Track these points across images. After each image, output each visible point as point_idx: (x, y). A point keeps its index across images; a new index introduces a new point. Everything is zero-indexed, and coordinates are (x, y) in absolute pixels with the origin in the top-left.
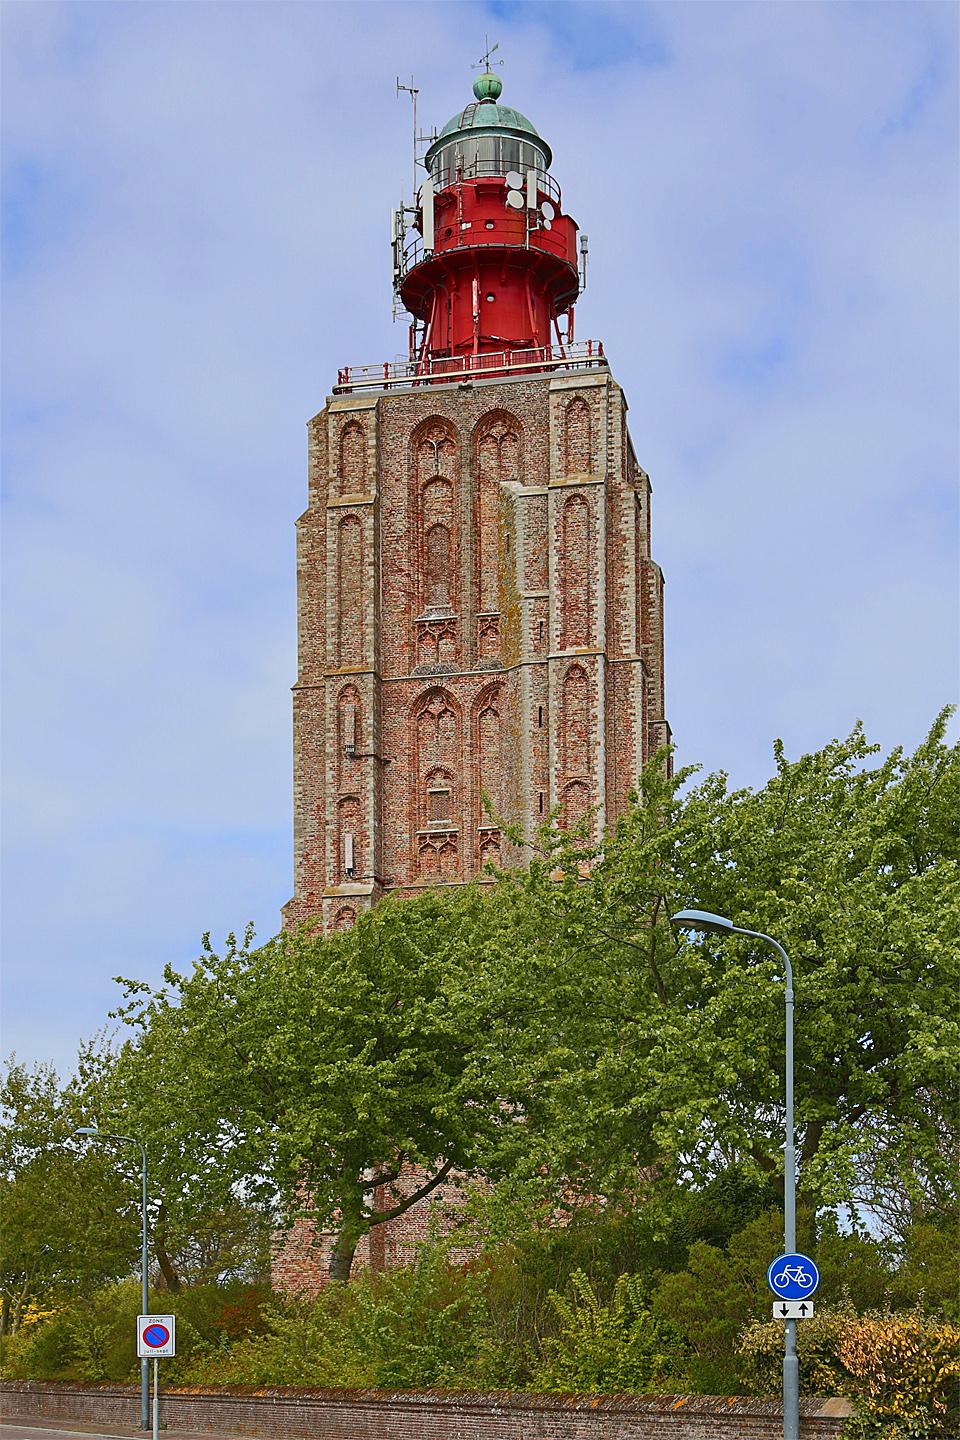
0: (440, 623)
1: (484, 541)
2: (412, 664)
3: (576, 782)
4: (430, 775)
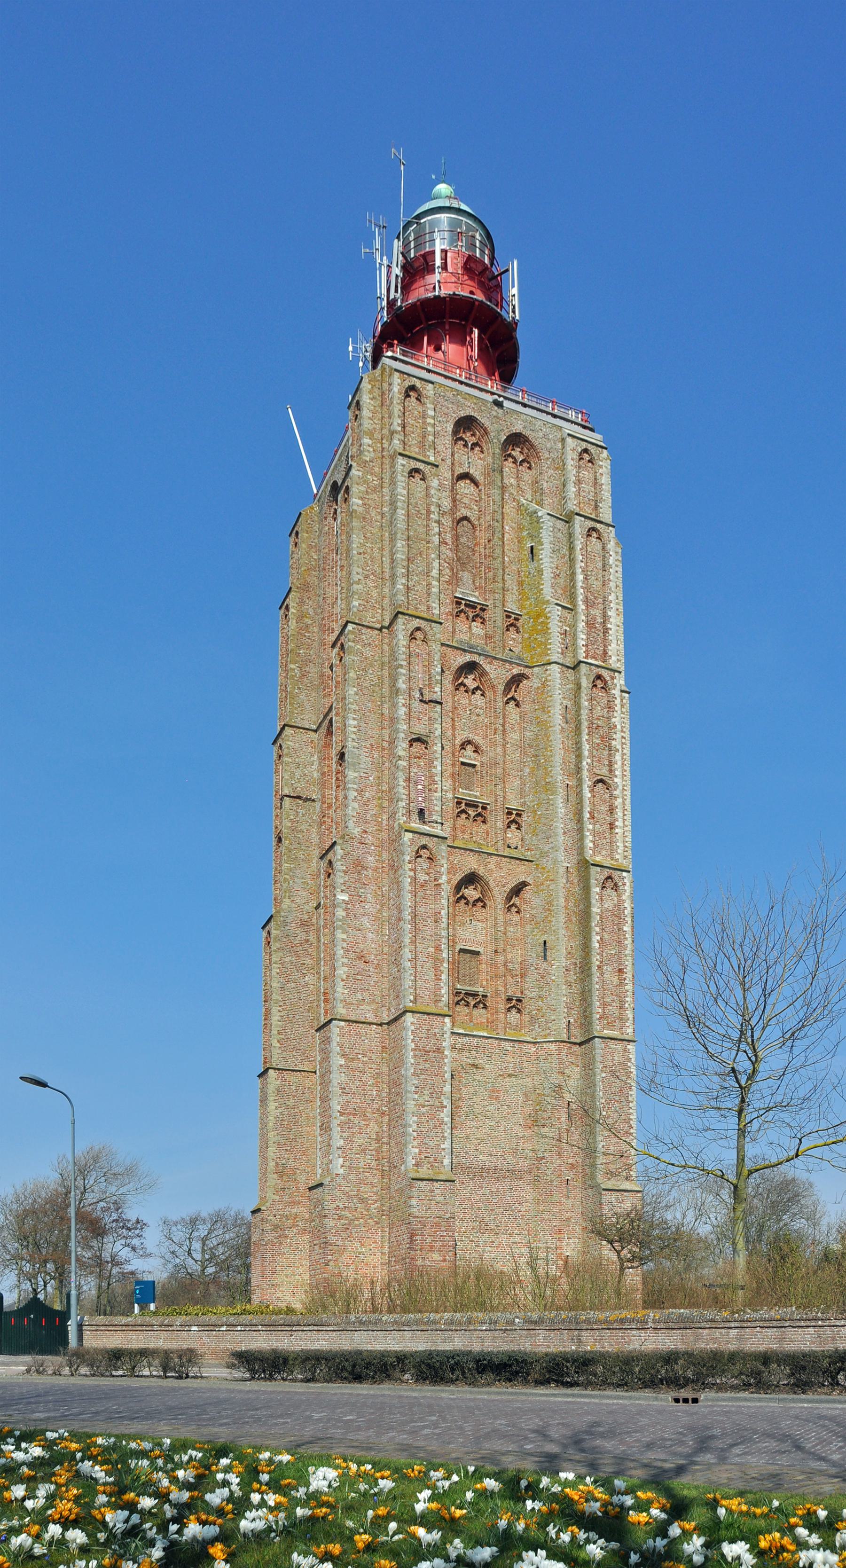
4: (463, 746)
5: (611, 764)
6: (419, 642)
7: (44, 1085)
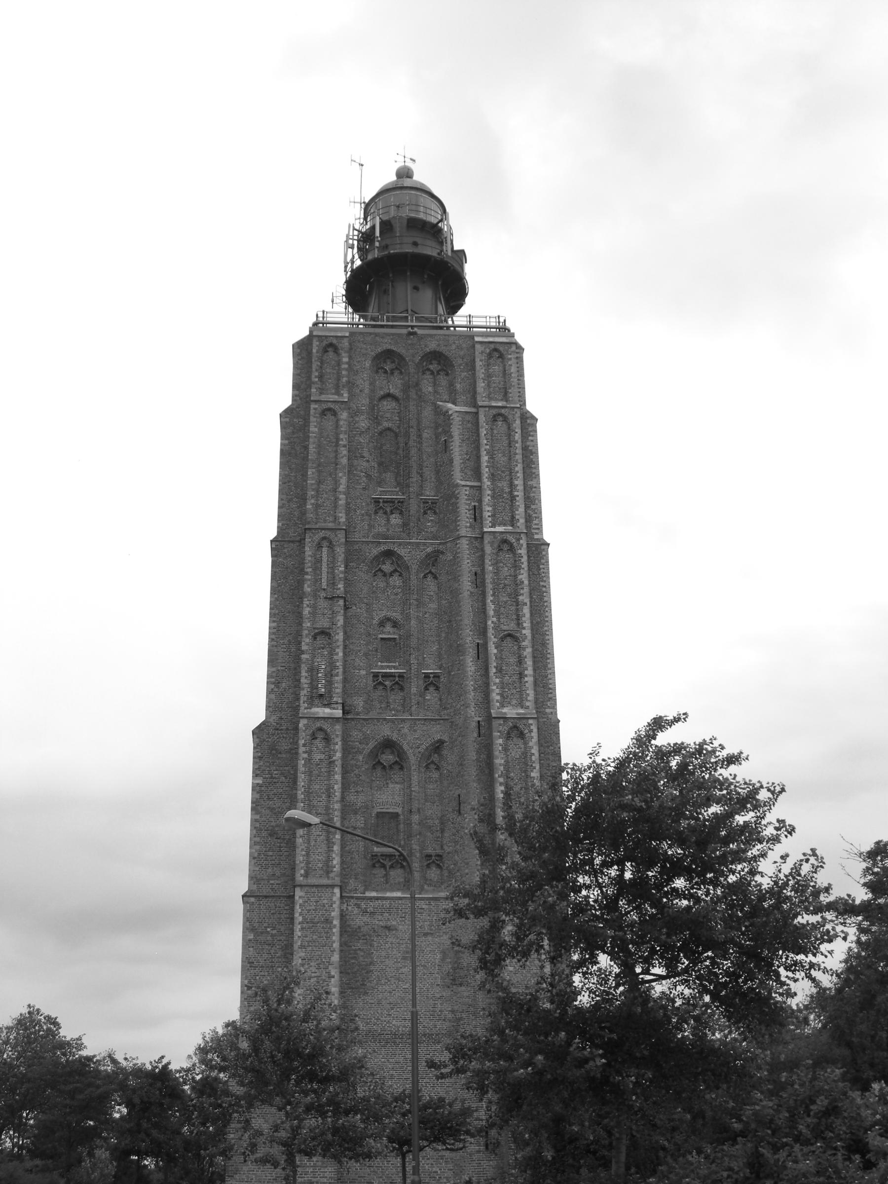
0: (392, 501)
1: (425, 444)
2: (369, 530)
3: (510, 635)
4: (382, 624)
5: (518, 618)
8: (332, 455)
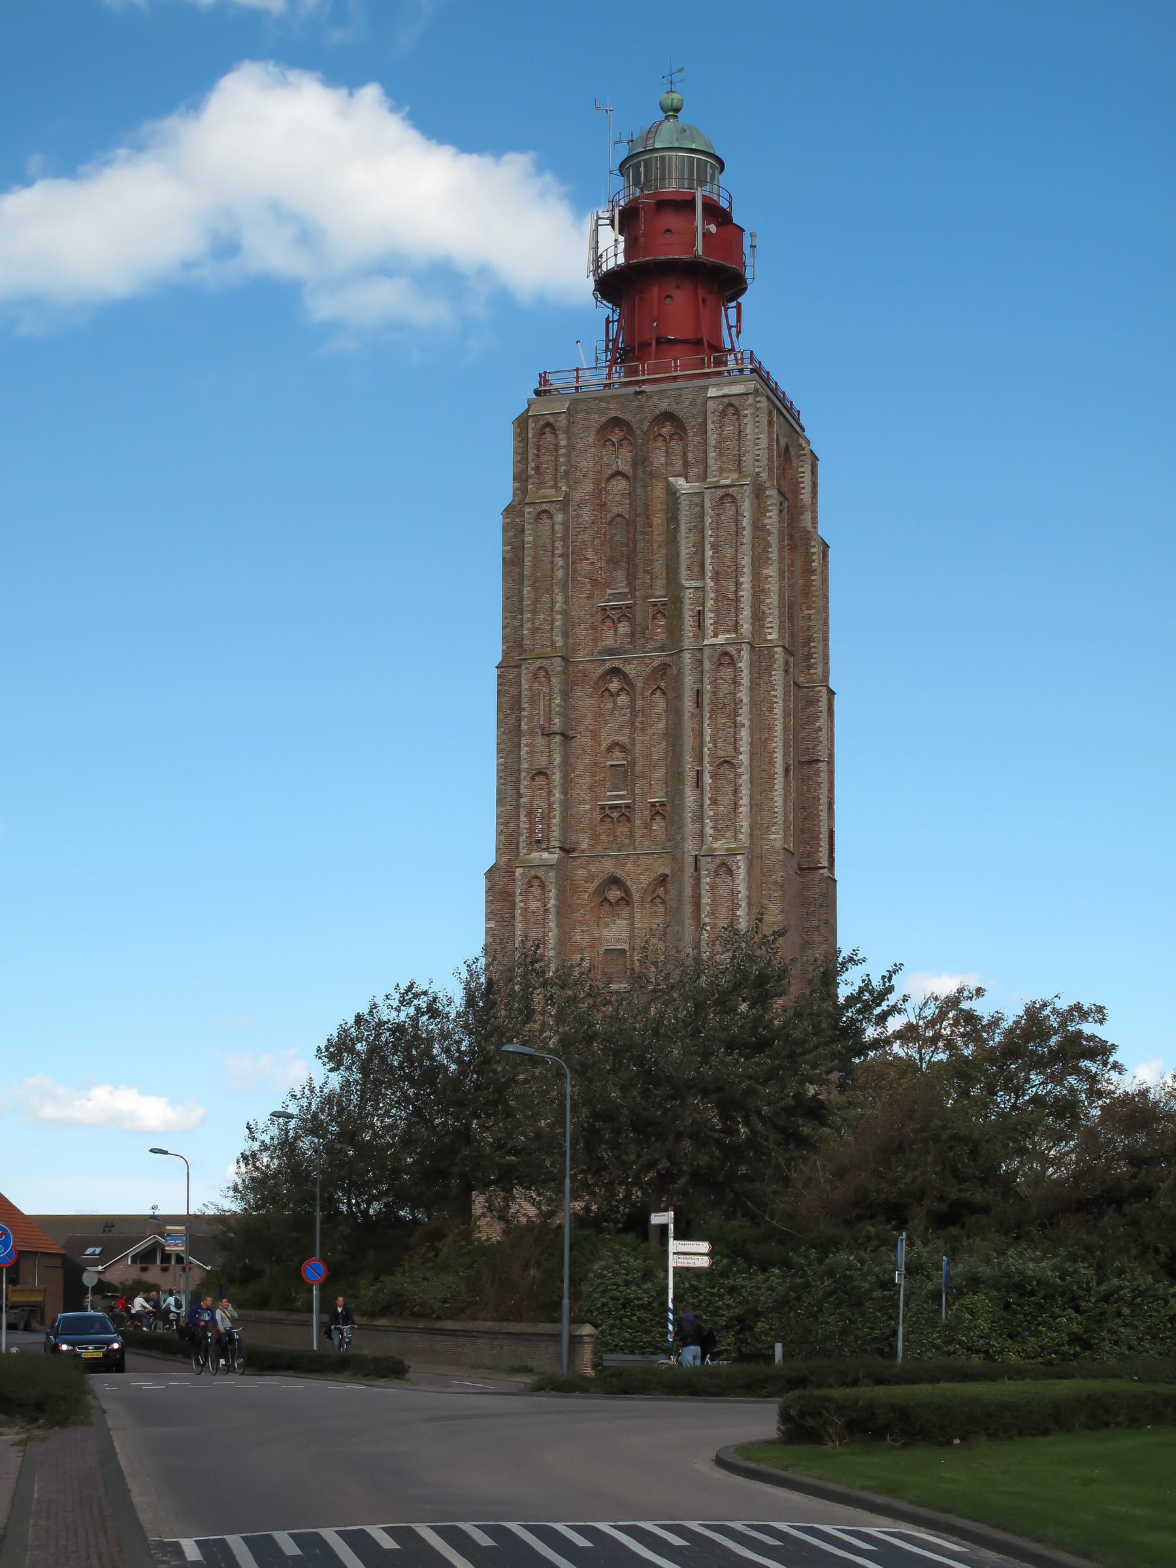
0: (619, 608)
1: (656, 532)
3: (726, 762)
4: (610, 749)
6: (543, 680)
7: (165, 1153)
8: (548, 567)
